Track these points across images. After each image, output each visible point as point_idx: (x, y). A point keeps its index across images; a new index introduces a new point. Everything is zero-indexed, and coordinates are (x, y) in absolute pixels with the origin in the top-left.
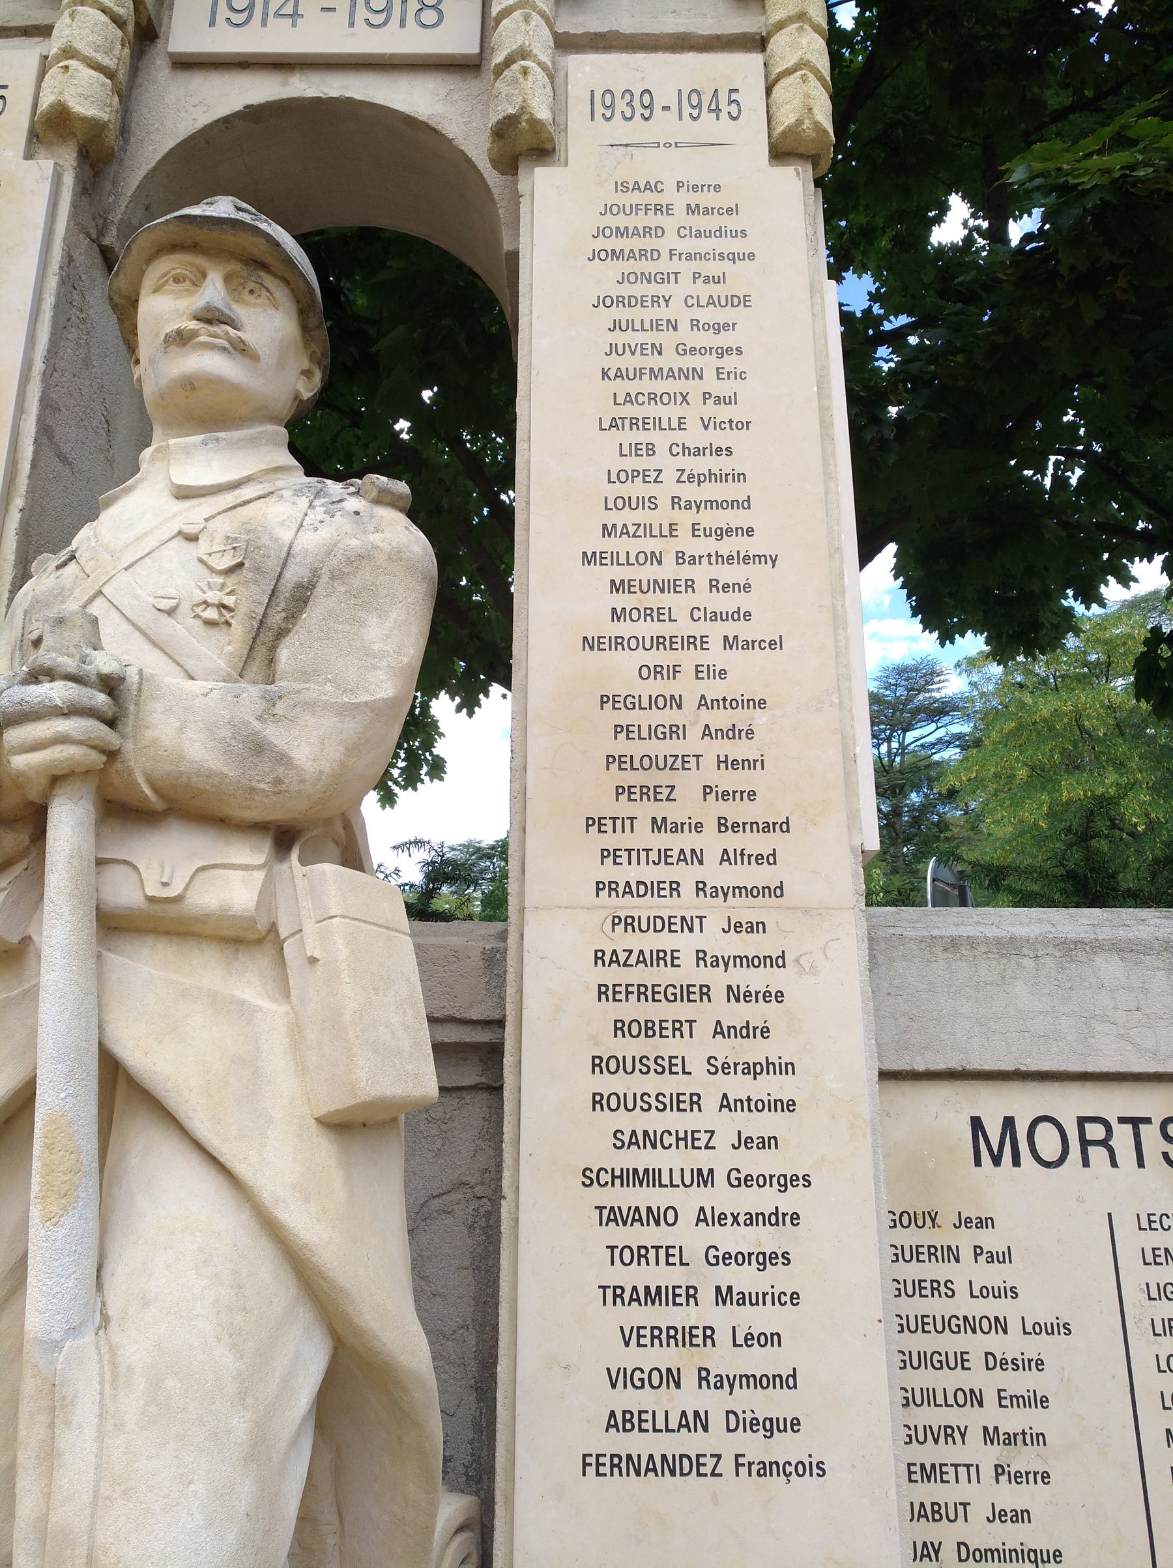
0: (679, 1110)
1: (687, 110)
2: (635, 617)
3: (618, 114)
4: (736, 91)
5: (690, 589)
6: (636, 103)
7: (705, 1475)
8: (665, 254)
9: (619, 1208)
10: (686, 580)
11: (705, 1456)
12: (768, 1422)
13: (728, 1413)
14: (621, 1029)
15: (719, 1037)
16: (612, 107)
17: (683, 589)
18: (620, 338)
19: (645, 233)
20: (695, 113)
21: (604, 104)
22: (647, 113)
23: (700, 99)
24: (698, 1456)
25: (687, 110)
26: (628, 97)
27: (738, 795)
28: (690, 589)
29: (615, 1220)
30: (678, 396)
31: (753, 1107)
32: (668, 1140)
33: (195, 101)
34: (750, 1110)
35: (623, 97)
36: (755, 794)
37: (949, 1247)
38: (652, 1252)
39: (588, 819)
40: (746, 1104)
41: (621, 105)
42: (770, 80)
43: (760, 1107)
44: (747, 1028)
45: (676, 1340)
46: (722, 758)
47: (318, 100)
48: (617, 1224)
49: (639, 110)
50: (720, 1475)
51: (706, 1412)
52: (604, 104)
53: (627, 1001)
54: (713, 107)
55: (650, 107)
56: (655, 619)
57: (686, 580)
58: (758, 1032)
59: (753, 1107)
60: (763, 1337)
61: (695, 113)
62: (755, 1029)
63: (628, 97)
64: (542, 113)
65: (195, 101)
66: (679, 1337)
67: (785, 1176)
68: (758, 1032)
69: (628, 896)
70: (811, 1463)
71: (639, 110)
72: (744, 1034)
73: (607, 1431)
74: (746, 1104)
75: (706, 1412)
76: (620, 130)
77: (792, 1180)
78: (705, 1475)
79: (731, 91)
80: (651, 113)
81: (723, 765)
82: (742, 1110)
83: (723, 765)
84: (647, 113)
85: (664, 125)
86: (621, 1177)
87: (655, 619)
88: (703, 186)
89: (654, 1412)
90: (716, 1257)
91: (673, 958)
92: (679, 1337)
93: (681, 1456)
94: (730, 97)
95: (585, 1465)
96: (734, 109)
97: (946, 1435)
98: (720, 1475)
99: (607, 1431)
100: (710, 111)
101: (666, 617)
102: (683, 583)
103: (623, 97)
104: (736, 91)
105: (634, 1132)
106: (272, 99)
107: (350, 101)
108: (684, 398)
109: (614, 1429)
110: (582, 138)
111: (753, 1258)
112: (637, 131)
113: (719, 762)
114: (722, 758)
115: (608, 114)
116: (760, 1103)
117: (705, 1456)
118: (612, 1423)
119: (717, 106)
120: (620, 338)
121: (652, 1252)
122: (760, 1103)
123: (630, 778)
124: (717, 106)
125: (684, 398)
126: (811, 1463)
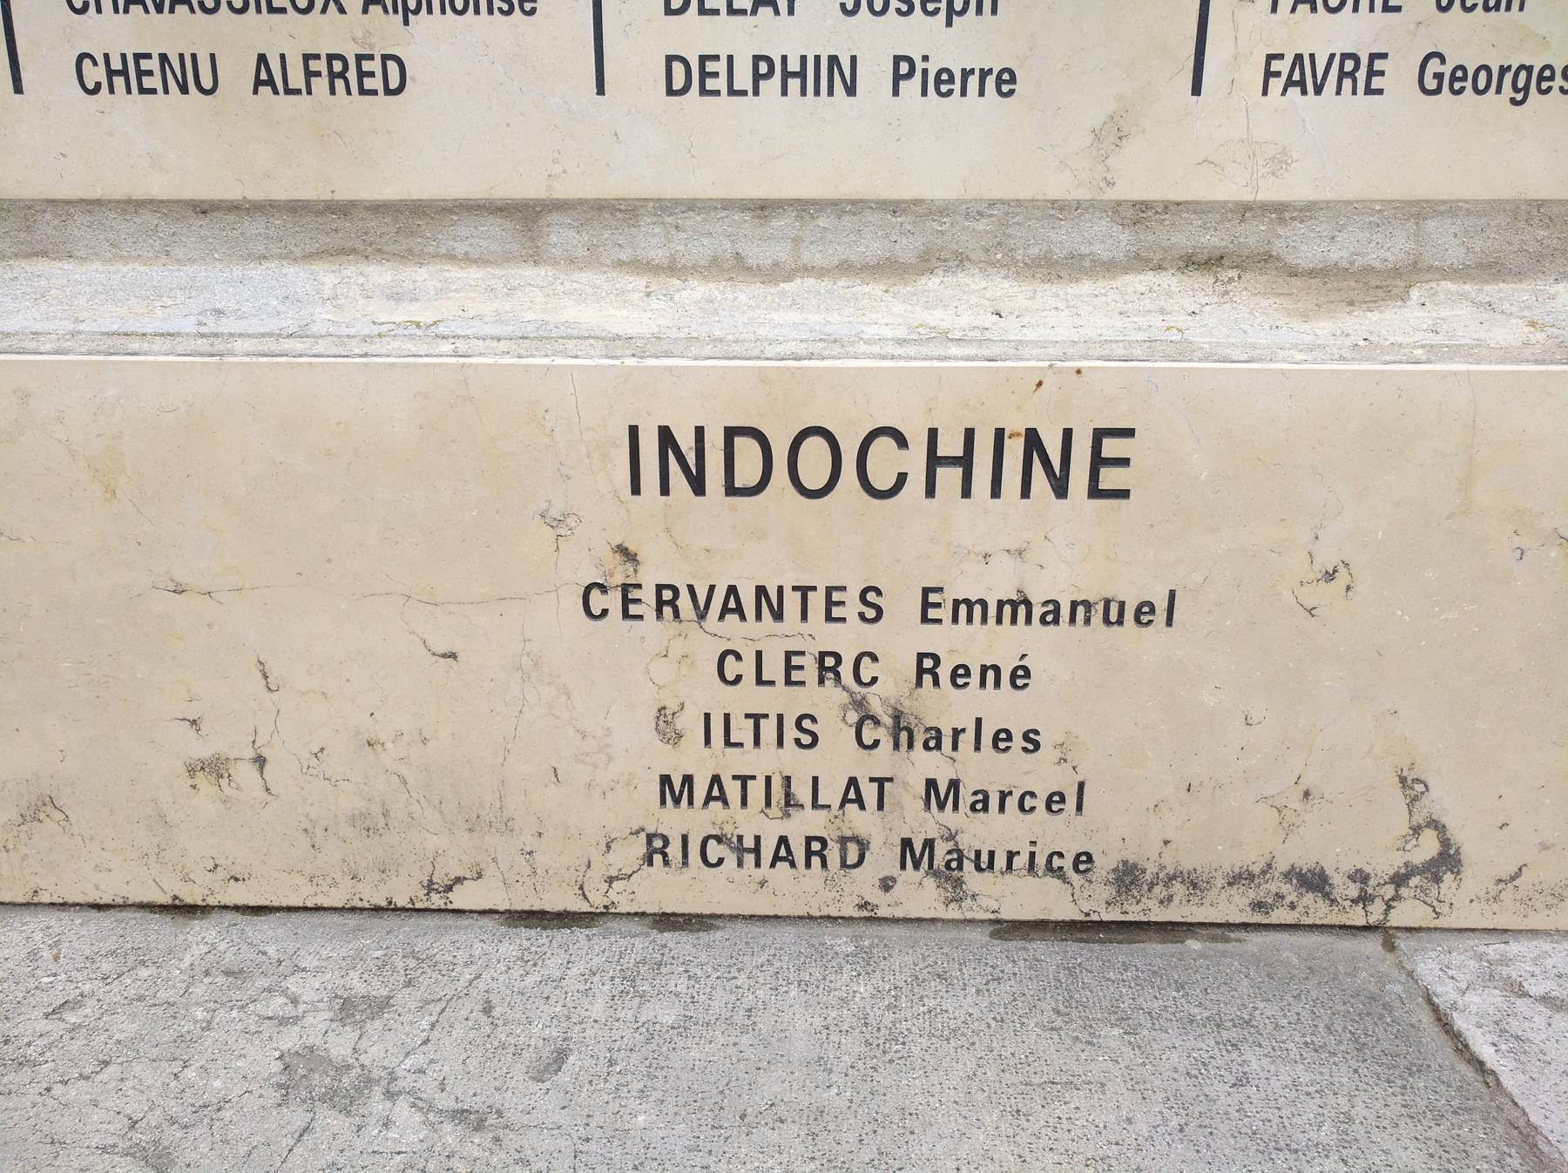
9: (1312, 56)
12: (1523, 75)
13: (670, 59)
19: (809, 854)
24: (703, 59)
37: (833, 60)
39: (897, 60)
48: (1304, 92)
51: (854, 59)
53: (756, 92)
60: (1483, 75)
69: (732, 618)
73: (255, 92)
75: (854, 59)
77: (1541, 79)
86: (802, 74)
88: (966, 74)
89: (730, 58)
90: (1439, 76)
91: (1372, 73)
95: (1269, 74)
97: (1342, 74)
99: (255, 92)
109: (736, 617)
111: (1508, 77)
118: (732, 604)
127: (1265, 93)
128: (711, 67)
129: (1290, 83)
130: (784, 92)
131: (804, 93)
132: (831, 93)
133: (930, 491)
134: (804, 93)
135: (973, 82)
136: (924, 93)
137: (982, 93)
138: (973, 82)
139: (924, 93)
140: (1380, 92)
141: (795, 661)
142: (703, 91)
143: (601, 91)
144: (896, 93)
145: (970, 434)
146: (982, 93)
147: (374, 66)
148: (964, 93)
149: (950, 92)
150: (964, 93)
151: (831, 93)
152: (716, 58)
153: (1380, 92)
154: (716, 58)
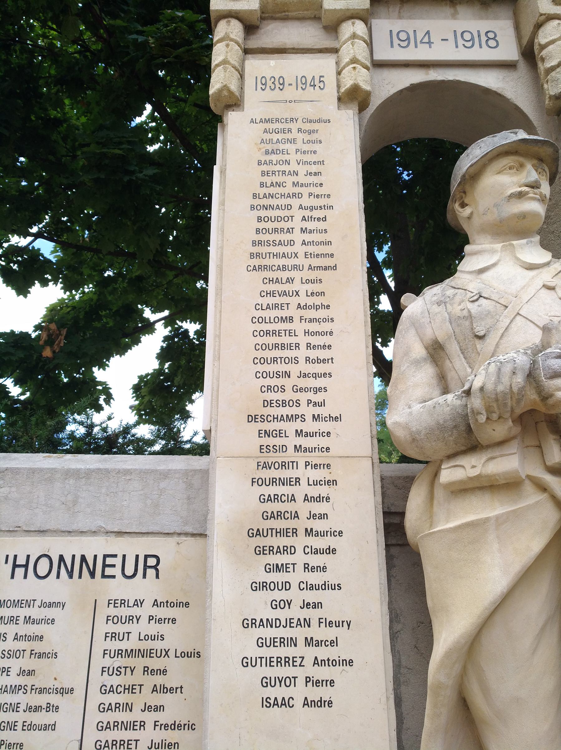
0: (287, 536)
1: (300, 85)
2: (281, 163)
3: (268, 87)
4: (323, 77)
5: (297, 348)
6: (277, 83)
7: (296, 666)
8: (295, 586)
10: (296, 344)
11: (296, 657)
14: (270, 389)
15: (306, 501)
16: (265, 84)
17: (294, 348)
18: (262, 225)
20: (304, 87)
21: (263, 83)
22: (281, 87)
23: (284, 81)
25: (300, 85)
26: (273, 80)
27: (322, 466)
28: (297, 348)
29: (266, 467)
30: (294, 292)
31: (330, 664)
32: (284, 498)
33: (386, 82)
34: (329, 666)
35: (270, 80)
36: (329, 449)
38: (279, 360)
40: (327, 662)
41: (269, 83)
42: (525, 41)
43: (334, 664)
44: (320, 497)
45: (284, 644)
46: (307, 331)
47: (443, 81)
49: (278, 85)
50: (304, 666)
52: (263, 83)
54: (312, 84)
55: (283, 84)
56: (280, 349)
57: (296, 344)
58: (325, 499)
59: (330, 664)
61: (304, 87)
62: (323, 498)
63: (273, 80)
64: (234, 87)
65: (386, 82)
66: (286, 642)
67: (316, 388)
68: (325, 499)
70: (339, 660)
71: (278, 85)
72: (323, 588)
73: (303, 707)
74: (327, 662)
76: (269, 94)
78: (296, 666)
79: (321, 77)
80: (283, 88)
81: (307, 334)
82: (325, 665)
83: (307, 334)
84: (281, 87)
85: (290, 93)
87: (280, 349)
90: (297, 389)
92: (286, 642)
93: (286, 582)
94: (320, 79)
96: (322, 85)
98: (304, 666)
99: (303, 707)
100: (311, 85)
101: (283, 435)
102: (294, 345)
103: (270, 80)
104: (323, 77)
105: (269, 495)
106: (422, 81)
107: (459, 82)
108: (296, 255)
110: (253, 98)
112: (276, 94)
113: (305, 332)
114: (307, 331)
115: (263, 87)
116: (334, 662)
117: (296, 657)
119: (314, 82)
120: (262, 225)
121: (279, 360)
122: (334, 662)
123: (268, 382)
124: (314, 82)
125: (296, 255)
126: (339, 660)
127: (12, 577)
128: (152, 651)
129: (263, 467)
130: (111, 640)
131: (281, 536)
132: (291, 646)
133: (28, 556)
134: (281, 536)
135: (167, 621)
136: (312, 468)
137: (168, 623)
138: (167, 621)
139: (312, 468)
140: (16, 730)
141: (262, 447)
142: (274, 646)
143: (96, 600)
144: (149, 623)
145: (144, 576)
146: (168, 623)
147: (274, 402)
148: (164, 623)
149: (181, 729)
150: (164, 623)
151: (291, 646)
152: (153, 649)
153: (16, 730)
154: (153, 649)
